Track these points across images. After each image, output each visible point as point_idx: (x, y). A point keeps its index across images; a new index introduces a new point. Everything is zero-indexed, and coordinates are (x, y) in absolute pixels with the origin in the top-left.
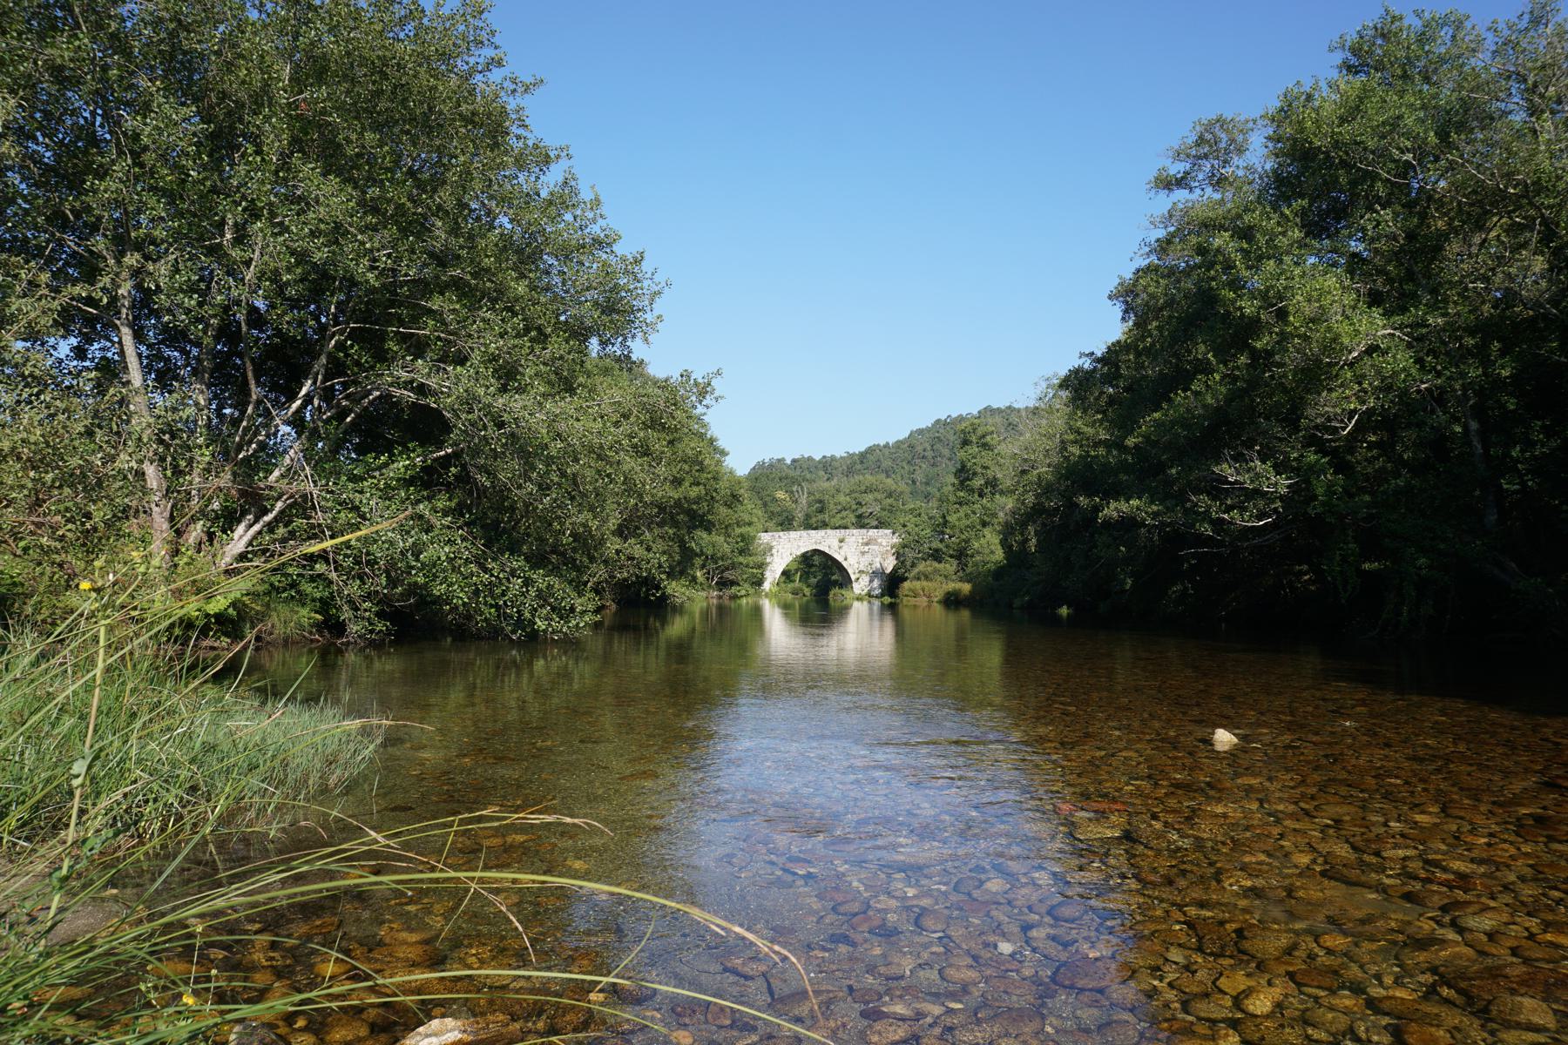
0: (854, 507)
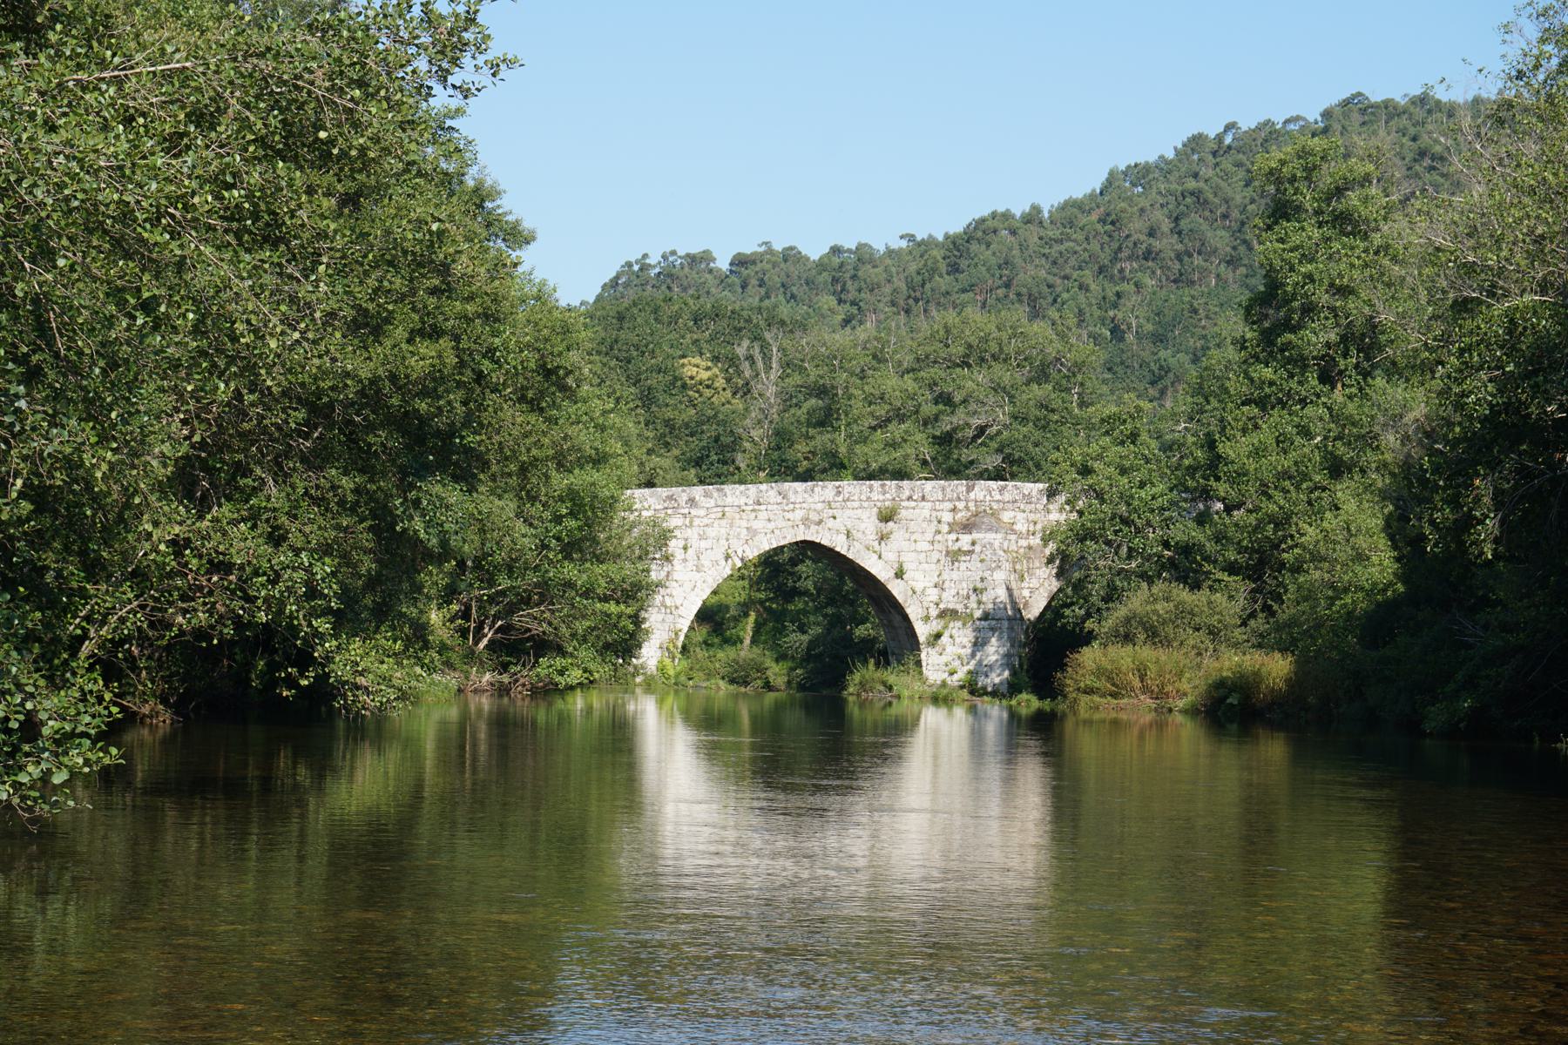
0: (928, 409)
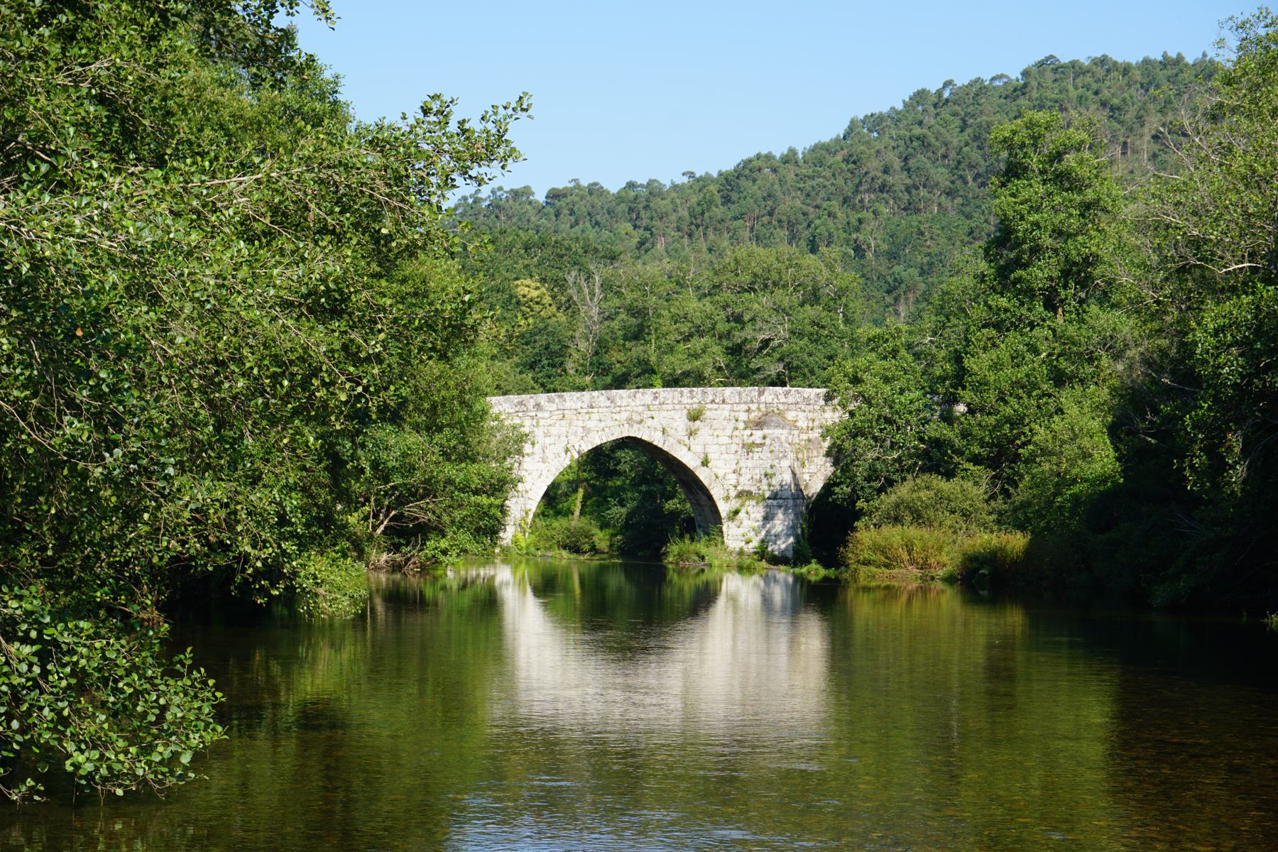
0: (722, 327)
